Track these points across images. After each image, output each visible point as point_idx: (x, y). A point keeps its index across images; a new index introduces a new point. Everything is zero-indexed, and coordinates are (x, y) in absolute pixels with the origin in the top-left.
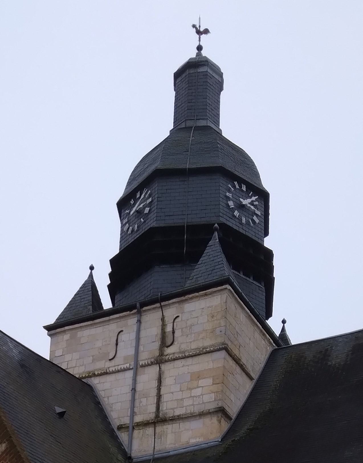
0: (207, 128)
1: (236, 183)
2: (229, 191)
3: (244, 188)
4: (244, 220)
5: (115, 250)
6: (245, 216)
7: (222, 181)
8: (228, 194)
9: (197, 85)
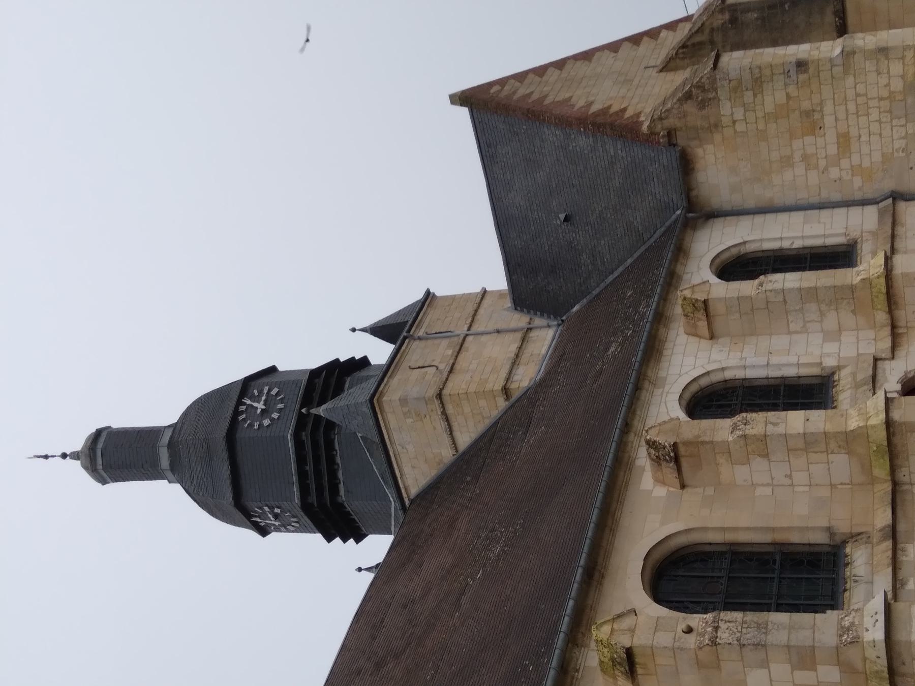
0: (171, 445)
1: (240, 418)
2: (251, 425)
3: (243, 408)
4: (280, 406)
5: (318, 537)
6: (275, 404)
7: (240, 435)
8: (256, 427)
9: (116, 455)
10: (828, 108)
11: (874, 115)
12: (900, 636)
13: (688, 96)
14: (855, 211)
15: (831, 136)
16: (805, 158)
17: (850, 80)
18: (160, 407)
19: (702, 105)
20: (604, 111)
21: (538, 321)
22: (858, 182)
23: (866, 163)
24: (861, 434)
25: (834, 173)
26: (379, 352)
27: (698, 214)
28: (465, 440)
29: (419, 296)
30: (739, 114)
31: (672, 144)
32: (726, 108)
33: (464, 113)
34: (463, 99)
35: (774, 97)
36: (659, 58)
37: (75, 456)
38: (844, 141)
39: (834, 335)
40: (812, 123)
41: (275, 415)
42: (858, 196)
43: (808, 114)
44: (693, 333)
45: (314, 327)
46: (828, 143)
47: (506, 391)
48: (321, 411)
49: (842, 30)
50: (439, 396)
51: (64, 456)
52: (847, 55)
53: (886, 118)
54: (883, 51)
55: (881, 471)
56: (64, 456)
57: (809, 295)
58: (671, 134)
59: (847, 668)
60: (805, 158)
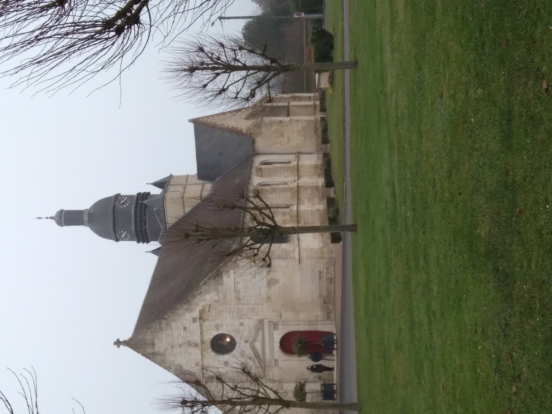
2: (120, 207)
5: (134, 243)
9: (68, 218)
10: (286, 132)
11: (295, 134)
12: (299, 209)
13: (255, 126)
14: (290, 155)
15: (286, 138)
16: (280, 143)
17: (291, 126)
18: (84, 203)
19: (258, 128)
20: (233, 127)
21: (206, 182)
22: (291, 149)
23: (293, 145)
24: (293, 188)
25: (286, 146)
26: (156, 191)
27: (256, 153)
28: (187, 210)
29: (169, 175)
30: (266, 131)
31: (251, 136)
32: (263, 129)
33: (192, 125)
34: (190, 121)
35: (274, 128)
36: (244, 116)
37: (52, 218)
38: (289, 139)
39: (287, 176)
40: (282, 135)
41: (127, 205)
42: (291, 152)
43: (281, 133)
44: (257, 175)
45: (135, 182)
46: (285, 140)
47: (201, 197)
48: (145, 202)
49: (288, 115)
50: (182, 198)
51: (47, 218)
52: (290, 120)
53: (298, 135)
54: (298, 121)
55: (296, 196)
56: (47, 218)
57: (282, 168)
58: (251, 134)
59: (291, 216)
60: (280, 143)
